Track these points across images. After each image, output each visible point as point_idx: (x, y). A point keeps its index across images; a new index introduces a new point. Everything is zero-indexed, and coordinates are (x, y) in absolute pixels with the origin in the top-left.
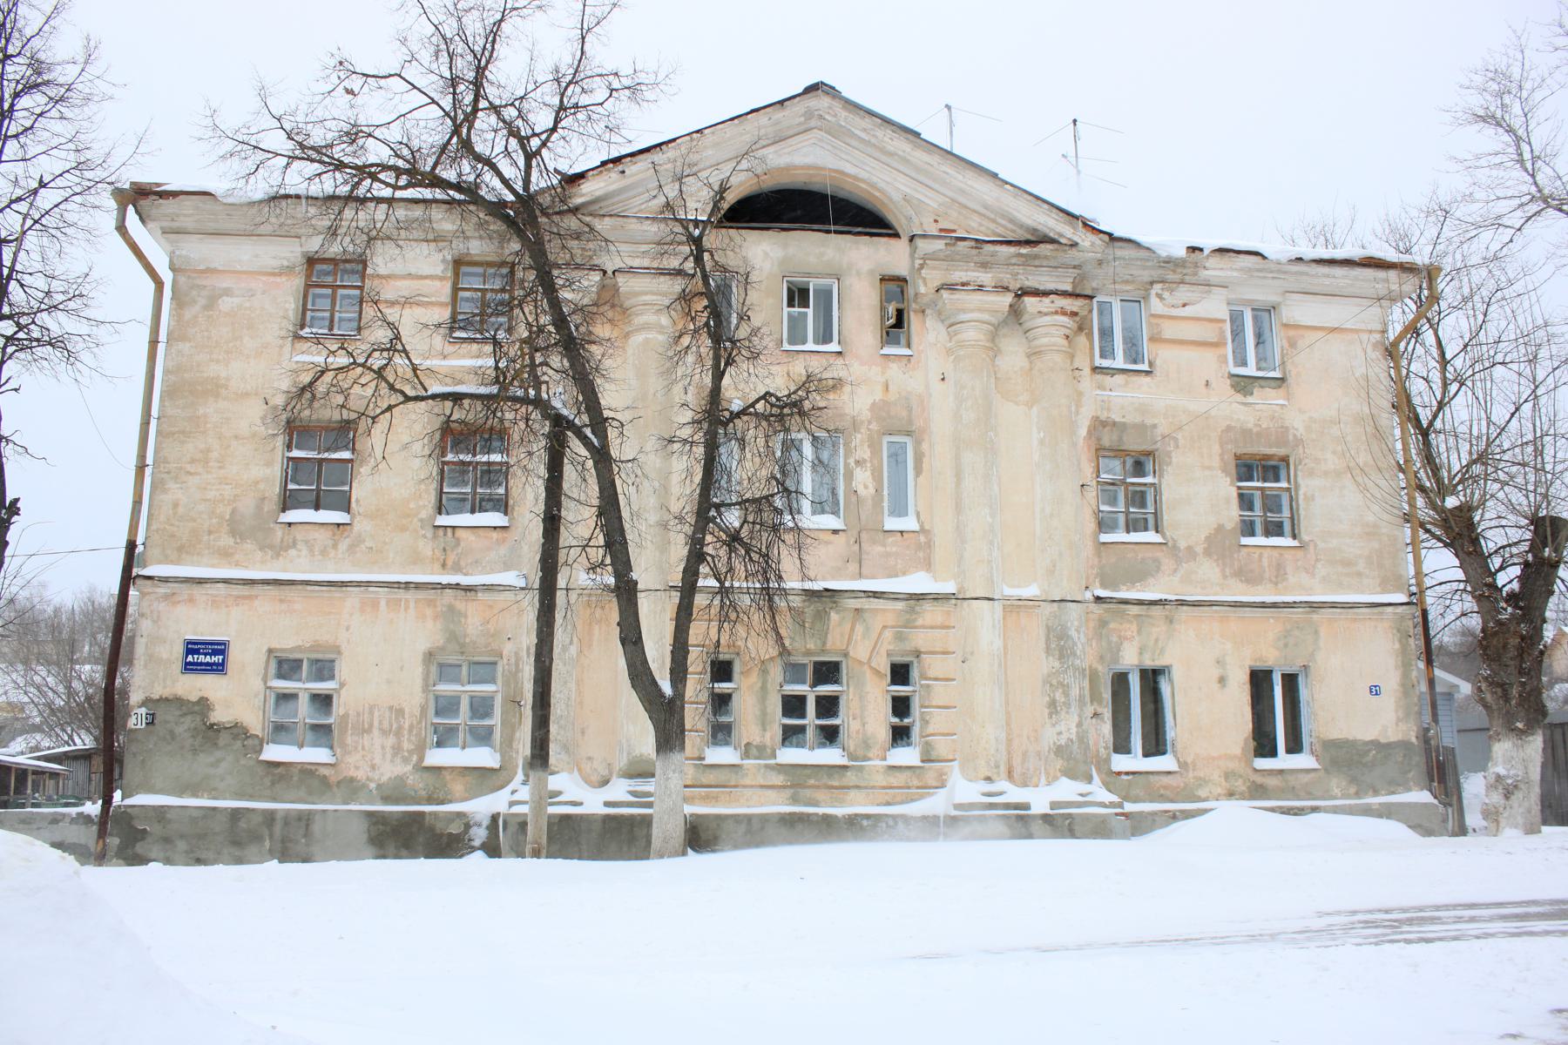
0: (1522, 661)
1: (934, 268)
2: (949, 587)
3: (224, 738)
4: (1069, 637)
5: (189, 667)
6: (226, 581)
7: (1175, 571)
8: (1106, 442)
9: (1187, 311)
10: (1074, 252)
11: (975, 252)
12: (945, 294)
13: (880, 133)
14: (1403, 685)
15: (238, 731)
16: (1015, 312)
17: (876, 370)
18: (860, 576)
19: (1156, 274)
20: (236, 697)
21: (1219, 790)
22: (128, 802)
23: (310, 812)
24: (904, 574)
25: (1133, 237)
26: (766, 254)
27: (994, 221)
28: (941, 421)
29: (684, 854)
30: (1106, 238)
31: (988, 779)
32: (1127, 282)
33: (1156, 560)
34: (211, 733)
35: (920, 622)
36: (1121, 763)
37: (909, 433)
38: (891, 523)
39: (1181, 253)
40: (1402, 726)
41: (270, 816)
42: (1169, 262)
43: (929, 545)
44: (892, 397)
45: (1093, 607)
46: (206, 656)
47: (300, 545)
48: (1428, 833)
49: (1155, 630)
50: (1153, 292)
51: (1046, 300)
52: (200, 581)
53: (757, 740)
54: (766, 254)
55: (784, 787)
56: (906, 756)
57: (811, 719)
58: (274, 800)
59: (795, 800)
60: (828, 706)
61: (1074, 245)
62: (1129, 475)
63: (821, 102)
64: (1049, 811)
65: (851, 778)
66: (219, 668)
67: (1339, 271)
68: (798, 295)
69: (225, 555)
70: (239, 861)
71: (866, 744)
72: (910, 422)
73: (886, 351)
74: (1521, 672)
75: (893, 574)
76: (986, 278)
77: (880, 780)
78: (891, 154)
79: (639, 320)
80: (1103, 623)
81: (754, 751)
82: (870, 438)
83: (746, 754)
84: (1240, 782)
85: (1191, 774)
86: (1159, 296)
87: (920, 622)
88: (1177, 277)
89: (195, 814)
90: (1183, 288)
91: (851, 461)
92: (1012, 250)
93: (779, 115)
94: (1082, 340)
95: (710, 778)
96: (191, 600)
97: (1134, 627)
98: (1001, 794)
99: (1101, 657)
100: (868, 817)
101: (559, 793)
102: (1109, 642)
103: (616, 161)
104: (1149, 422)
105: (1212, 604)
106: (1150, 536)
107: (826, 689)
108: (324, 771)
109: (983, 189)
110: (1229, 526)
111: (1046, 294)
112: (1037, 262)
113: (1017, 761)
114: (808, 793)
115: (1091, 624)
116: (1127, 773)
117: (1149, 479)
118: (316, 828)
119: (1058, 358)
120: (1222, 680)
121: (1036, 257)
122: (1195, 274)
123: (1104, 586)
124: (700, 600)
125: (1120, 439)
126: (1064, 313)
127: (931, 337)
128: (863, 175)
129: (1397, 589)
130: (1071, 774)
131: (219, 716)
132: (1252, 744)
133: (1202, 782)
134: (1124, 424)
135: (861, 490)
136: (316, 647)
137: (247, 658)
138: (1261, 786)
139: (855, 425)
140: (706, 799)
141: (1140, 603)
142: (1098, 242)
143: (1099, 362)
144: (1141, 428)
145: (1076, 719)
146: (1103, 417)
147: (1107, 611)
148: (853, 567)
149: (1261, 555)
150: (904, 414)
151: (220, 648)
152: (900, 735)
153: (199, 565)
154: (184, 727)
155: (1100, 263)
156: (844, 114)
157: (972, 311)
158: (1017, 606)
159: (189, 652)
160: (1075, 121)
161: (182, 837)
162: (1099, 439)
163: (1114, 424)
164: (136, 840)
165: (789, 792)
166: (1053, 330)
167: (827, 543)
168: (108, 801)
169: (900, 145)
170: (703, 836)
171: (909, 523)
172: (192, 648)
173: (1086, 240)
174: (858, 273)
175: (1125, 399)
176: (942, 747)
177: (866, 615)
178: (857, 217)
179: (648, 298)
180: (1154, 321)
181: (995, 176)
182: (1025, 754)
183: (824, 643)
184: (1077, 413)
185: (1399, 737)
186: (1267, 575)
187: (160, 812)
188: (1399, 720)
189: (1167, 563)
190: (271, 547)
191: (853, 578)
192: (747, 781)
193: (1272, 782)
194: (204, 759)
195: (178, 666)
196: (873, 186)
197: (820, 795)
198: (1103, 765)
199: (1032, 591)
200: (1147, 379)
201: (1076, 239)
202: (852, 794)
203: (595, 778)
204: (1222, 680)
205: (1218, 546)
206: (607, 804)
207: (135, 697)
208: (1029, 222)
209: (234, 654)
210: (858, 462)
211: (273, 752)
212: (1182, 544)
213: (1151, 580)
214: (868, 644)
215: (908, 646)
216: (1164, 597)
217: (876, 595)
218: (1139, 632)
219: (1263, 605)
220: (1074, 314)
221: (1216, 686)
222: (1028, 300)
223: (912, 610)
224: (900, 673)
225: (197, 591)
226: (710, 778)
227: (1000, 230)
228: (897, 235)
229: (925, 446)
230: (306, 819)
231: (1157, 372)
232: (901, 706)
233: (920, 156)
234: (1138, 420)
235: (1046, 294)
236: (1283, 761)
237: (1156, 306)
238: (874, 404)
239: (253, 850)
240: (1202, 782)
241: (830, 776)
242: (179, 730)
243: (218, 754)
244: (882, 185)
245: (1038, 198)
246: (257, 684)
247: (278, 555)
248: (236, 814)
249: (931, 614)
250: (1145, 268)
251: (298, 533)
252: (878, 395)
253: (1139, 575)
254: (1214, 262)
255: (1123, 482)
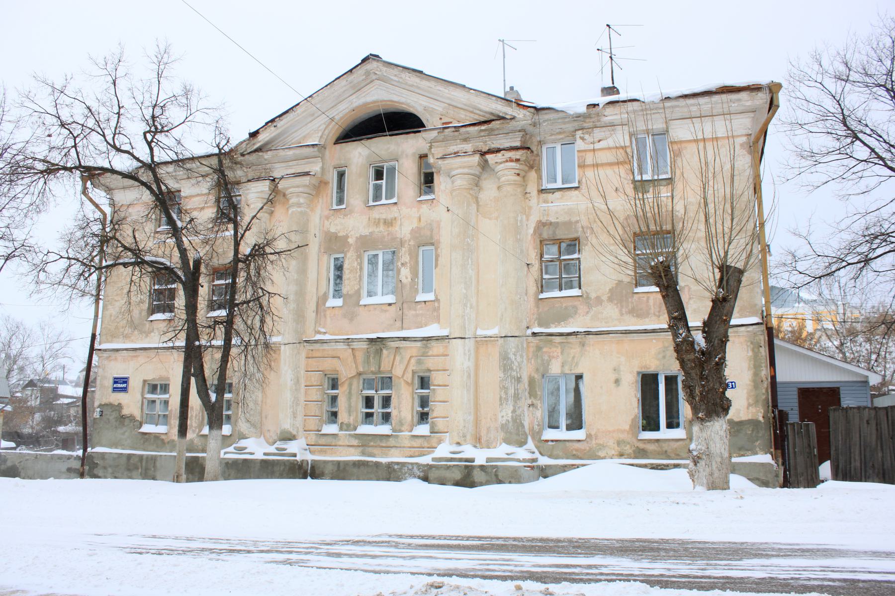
0: (703, 369)
1: (438, 147)
2: (445, 333)
3: (127, 422)
4: (509, 358)
5: (115, 390)
6: (126, 350)
7: (587, 313)
8: (545, 236)
9: (603, 144)
10: (513, 123)
11: (456, 133)
12: (440, 162)
13: (403, 75)
14: (754, 381)
15: (132, 418)
16: (484, 165)
17: (414, 210)
18: (402, 328)
19: (576, 125)
20: (131, 402)
21: (613, 452)
22: (94, 450)
23: (156, 456)
24: (426, 325)
25: (551, 106)
26: (360, 153)
27: (472, 112)
28: (447, 235)
29: (538, 479)
30: (532, 110)
31: (458, 444)
32: (560, 133)
33: (575, 307)
34: (123, 419)
35: (430, 353)
36: (550, 434)
37: (432, 244)
38: (421, 297)
39: (583, 109)
40: (752, 410)
41: (141, 456)
42: (579, 116)
43: (437, 310)
44: (422, 224)
45: (531, 339)
46: (121, 384)
47: (155, 331)
48: (765, 484)
49: (573, 351)
50: (578, 136)
51: (499, 155)
52: (117, 350)
53: (346, 421)
54: (360, 153)
55: (359, 446)
56: (423, 430)
57: (377, 409)
58: (144, 450)
59: (363, 454)
60: (386, 401)
61: (513, 118)
62: (559, 254)
63: (372, 65)
64: (484, 463)
65: (392, 442)
66: (124, 390)
67: (702, 100)
68: (379, 175)
69: (126, 337)
70: (130, 478)
71: (401, 423)
72: (432, 237)
73: (423, 198)
74: (702, 378)
75: (419, 326)
76: (468, 147)
77: (407, 443)
78: (412, 86)
79: (291, 201)
80: (539, 348)
81: (345, 427)
82: (410, 250)
83: (341, 429)
84: (628, 447)
85: (594, 442)
86: (582, 139)
87: (430, 353)
88: (591, 125)
89: (116, 456)
90: (596, 131)
91: (399, 264)
92: (476, 128)
93: (351, 78)
94: (533, 174)
95: (323, 441)
96: (116, 359)
97: (559, 350)
98: (460, 452)
99: (537, 370)
100: (398, 463)
101: (245, 448)
102: (543, 360)
103: (272, 121)
104: (574, 219)
105: (609, 333)
106: (575, 292)
107: (386, 392)
108: (163, 437)
109: (460, 96)
110: (627, 279)
111: (498, 151)
112: (496, 133)
113: (483, 433)
114: (370, 450)
115: (531, 349)
116: (552, 441)
117: (575, 256)
118: (158, 464)
119: (509, 189)
120: (617, 382)
121: (492, 130)
122: (599, 121)
123: (540, 325)
124: (234, 351)
125: (554, 233)
126: (511, 161)
127: (442, 187)
128: (403, 100)
129: (753, 314)
130: (508, 441)
131: (126, 412)
132: (640, 422)
133: (602, 447)
134: (558, 223)
135: (404, 280)
136: (161, 378)
137: (135, 384)
138: (643, 450)
139: (402, 243)
140: (321, 452)
141: (561, 335)
142: (528, 114)
143: (546, 185)
144: (568, 224)
145: (512, 408)
146: (544, 221)
147: (540, 340)
148: (399, 324)
149: (648, 298)
150: (429, 233)
151: (125, 380)
152: (423, 417)
153: (118, 342)
154: (113, 416)
155: (534, 125)
156: (385, 69)
157: (457, 169)
158: (482, 342)
159: (115, 382)
160: (608, 25)
161: (110, 466)
162: (540, 235)
163: (551, 223)
164: (94, 468)
165: (360, 449)
166: (506, 172)
167: (386, 311)
168: (85, 450)
169: (414, 79)
170: (317, 472)
171: (430, 297)
172: (116, 381)
173: (520, 114)
174: (407, 156)
175: (558, 208)
176: (441, 424)
177: (401, 351)
178: (401, 122)
179: (291, 190)
180: (581, 154)
181: (464, 86)
182: (488, 429)
183: (379, 368)
184: (528, 220)
185: (750, 417)
186: (652, 311)
187: (103, 454)
188: (749, 405)
189: (582, 308)
190: (145, 332)
191: (398, 330)
192: (340, 443)
193: (651, 447)
194: (120, 431)
195: (111, 389)
196: (408, 105)
197: (376, 451)
198: (536, 435)
199: (494, 331)
200: (577, 192)
201: (514, 114)
202: (393, 450)
203: (271, 440)
204: (617, 382)
205: (618, 295)
206: (265, 454)
207: (96, 404)
208: (487, 109)
209: (132, 383)
210: (402, 264)
211: (147, 428)
212: (593, 295)
213: (571, 320)
214: (403, 367)
215: (424, 367)
216: (576, 330)
217: (404, 339)
218: (562, 353)
219: (646, 332)
220: (518, 160)
221: (613, 385)
222: (489, 157)
223: (426, 347)
224: (424, 383)
225: (118, 354)
226: (323, 441)
227: (476, 117)
228: (337, 142)
229: (439, 251)
230: (154, 459)
231: (583, 187)
232: (424, 402)
233: (425, 84)
234: (567, 219)
235: (498, 151)
236: (664, 433)
237: (580, 145)
238: (412, 230)
239: (134, 473)
240: (602, 447)
241: (381, 441)
242: (111, 418)
243: (125, 429)
244: (412, 104)
245: (489, 94)
246: (139, 397)
247: (147, 336)
248: (129, 456)
249: (436, 348)
250: (564, 123)
251: (155, 325)
252: (415, 225)
253: (562, 318)
254: (610, 110)
255: (559, 259)
